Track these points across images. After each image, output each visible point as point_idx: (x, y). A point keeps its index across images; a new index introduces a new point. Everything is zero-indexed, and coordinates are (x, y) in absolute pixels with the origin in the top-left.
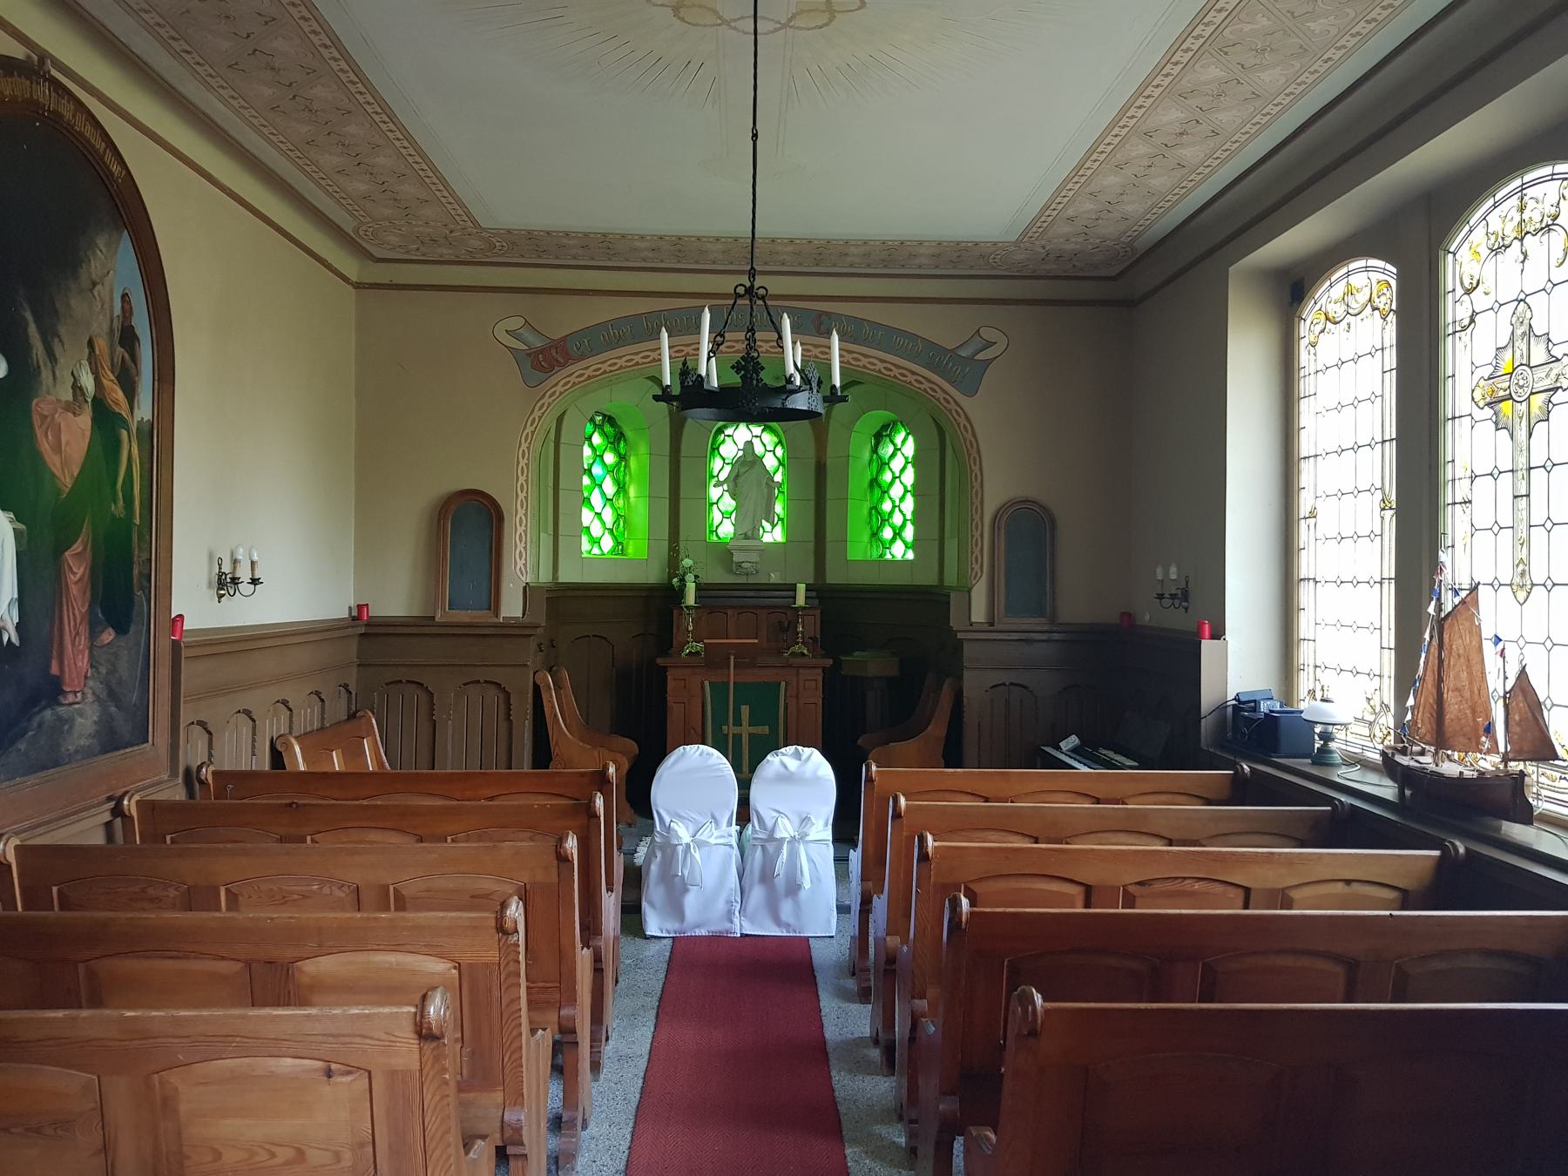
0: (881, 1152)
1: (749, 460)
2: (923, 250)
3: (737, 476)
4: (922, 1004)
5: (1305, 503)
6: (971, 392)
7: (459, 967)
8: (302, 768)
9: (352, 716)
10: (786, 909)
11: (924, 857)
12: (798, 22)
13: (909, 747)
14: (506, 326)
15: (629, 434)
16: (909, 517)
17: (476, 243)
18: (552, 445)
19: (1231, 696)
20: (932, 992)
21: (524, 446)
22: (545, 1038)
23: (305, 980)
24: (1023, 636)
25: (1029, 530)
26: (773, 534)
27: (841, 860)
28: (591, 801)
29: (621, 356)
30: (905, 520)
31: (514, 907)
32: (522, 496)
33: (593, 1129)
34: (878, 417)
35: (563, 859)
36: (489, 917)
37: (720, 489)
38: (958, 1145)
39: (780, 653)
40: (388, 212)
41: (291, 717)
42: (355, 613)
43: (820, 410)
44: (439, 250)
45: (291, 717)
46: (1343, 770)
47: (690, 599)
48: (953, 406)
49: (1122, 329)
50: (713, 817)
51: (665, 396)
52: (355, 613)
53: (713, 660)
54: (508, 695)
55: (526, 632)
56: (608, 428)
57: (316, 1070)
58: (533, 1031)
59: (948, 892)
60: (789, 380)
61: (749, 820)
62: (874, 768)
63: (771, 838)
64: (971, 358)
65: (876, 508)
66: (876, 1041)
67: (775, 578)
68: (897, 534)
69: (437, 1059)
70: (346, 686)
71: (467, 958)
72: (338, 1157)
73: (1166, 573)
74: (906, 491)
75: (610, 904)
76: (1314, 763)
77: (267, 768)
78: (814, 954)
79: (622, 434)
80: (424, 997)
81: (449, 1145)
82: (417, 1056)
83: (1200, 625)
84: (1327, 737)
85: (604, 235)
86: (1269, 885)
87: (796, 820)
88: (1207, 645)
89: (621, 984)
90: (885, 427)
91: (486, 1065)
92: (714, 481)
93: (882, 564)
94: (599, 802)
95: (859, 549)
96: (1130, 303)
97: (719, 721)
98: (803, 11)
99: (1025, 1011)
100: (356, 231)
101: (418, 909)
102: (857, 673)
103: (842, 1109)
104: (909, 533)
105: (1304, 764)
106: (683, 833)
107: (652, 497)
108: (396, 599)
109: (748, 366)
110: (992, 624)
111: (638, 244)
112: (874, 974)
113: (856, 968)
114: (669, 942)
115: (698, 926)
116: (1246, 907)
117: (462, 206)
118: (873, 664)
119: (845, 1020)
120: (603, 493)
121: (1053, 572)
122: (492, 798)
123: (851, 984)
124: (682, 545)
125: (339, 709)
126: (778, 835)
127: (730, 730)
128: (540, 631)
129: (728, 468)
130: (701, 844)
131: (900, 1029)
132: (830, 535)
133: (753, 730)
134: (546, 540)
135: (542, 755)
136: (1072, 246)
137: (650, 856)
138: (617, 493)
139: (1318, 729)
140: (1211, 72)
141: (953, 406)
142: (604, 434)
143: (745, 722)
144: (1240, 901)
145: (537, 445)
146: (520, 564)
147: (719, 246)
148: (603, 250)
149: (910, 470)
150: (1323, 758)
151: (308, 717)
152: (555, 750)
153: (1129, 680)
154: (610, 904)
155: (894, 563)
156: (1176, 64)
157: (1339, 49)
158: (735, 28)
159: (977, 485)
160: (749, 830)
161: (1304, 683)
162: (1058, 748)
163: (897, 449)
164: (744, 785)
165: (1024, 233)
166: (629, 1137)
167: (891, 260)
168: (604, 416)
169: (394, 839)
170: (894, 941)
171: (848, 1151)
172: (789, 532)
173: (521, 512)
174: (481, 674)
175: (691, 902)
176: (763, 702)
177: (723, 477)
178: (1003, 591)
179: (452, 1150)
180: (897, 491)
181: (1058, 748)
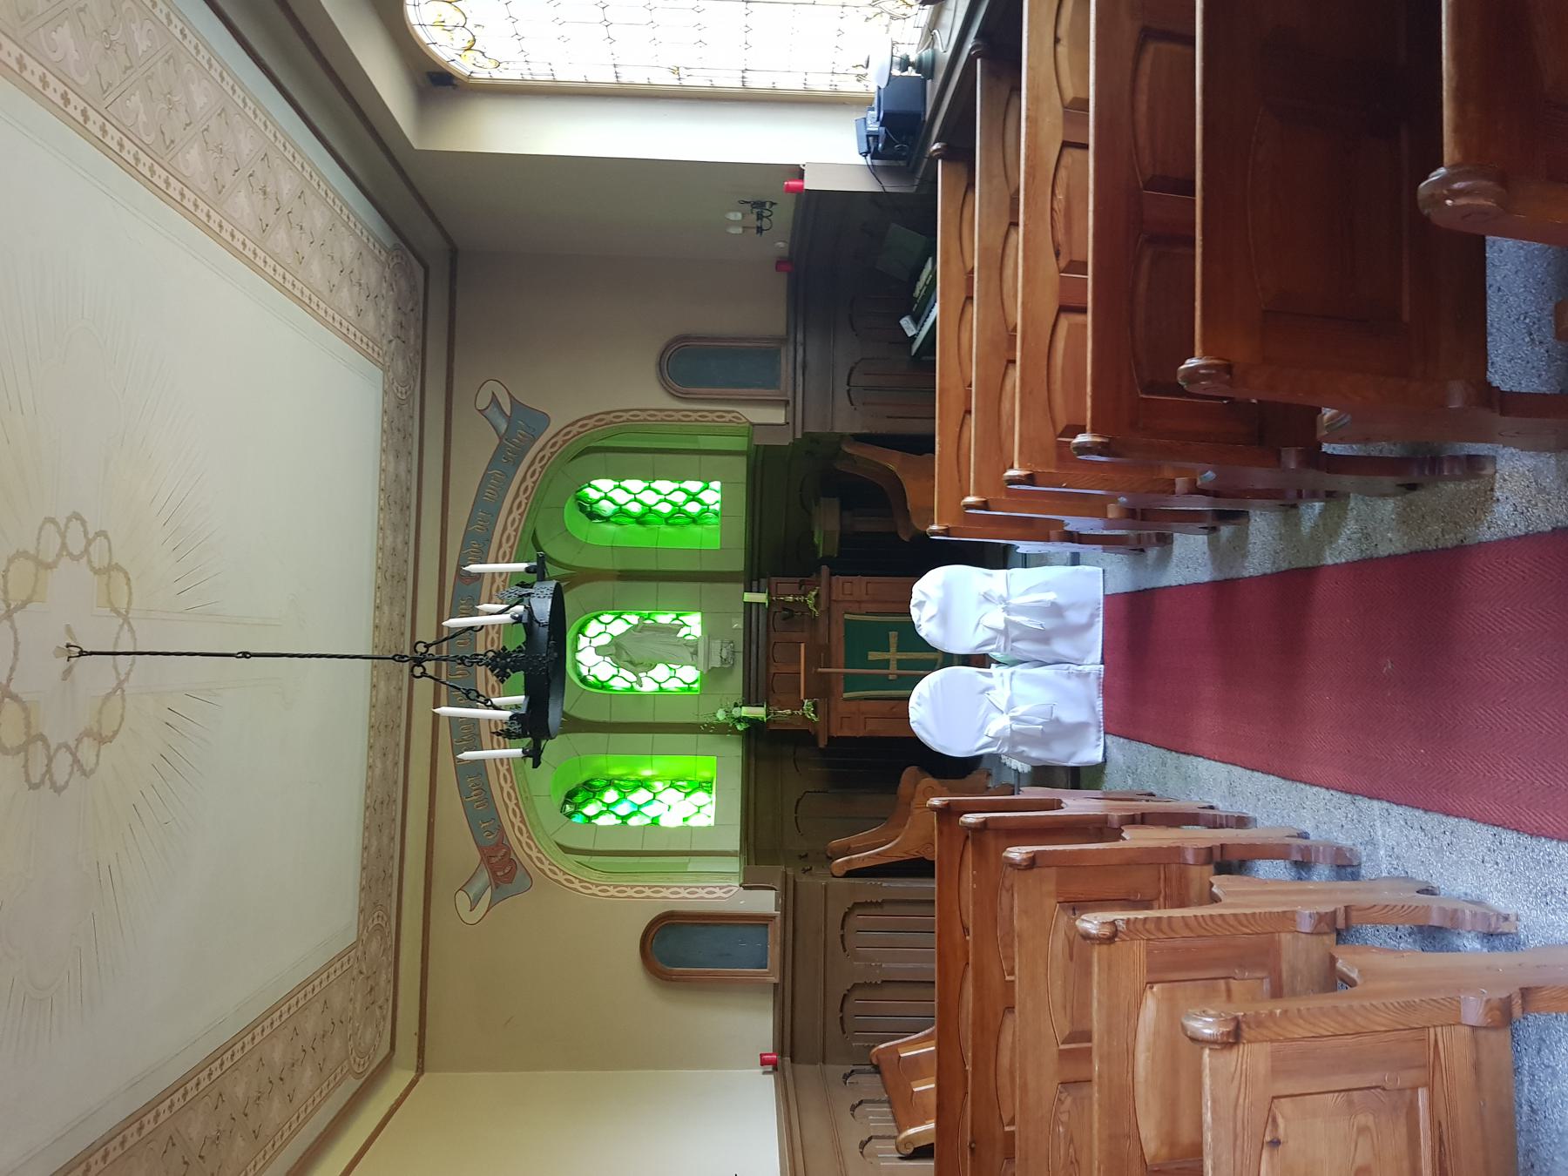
0: (1329, 529)
1: (616, 651)
2: (391, 468)
3: (631, 662)
4: (1181, 483)
5: (664, 79)
6: (546, 420)
7: (1151, 983)
8: (931, 1125)
9: (877, 1069)
10: (1076, 617)
11: (1030, 479)
12: (122, 605)
13: (912, 489)
14: (465, 911)
15: (585, 776)
16: (676, 485)
17: (374, 946)
18: (595, 859)
19: (862, 161)
20: (1167, 473)
21: (595, 890)
22: (1221, 884)
23: (1164, 1152)
24: (799, 372)
25: (690, 364)
26: (693, 625)
27: (1025, 562)
28: (969, 827)
29: (499, 789)
30: (679, 489)
31: (1088, 926)
32: (648, 892)
33: (1307, 827)
34: (572, 518)
35: (1032, 862)
36: (1097, 953)
37: (645, 680)
38: (1327, 448)
39: (814, 620)
40: (337, 1043)
41: (878, 1137)
42: (770, 1068)
43: (552, 584)
44: (382, 983)
45: (878, 1137)
46: (939, 48)
47: (759, 712)
48: (560, 439)
49: (471, 260)
50: (983, 692)
51: (535, 755)
52: (770, 1068)
53: (822, 690)
54: (856, 905)
55: (791, 886)
56: (579, 799)
57: (1271, 1157)
58: (1214, 899)
59: (1065, 455)
60: (518, 620)
61: (985, 656)
62: (935, 527)
63: (1005, 633)
64: (509, 419)
65: (666, 520)
66: (1213, 530)
67: (738, 624)
68: (694, 498)
69: (1260, 1024)
70: (846, 1077)
71: (1141, 976)
72: (1363, 1130)
73: (735, 223)
74: (649, 488)
75: (1076, 804)
76: (932, 77)
77: (932, 1163)
78: (1121, 590)
79: (585, 783)
80: (1194, 1039)
81: (1351, 1007)
82: (1256, 1046)
83: (789, 189)
84: (905, 64)
85: (367, 808)
86: (1059, 121)
87: (987, 606)
88: (810, 183)
89: (1153, 789)
90: (582, 509)
91: (1250, 953)
92: (636, 687)
93: (724, 514)
94: (971, 818)
95: (708, 537)
96: (454, 253)
97: (884, 682)
98: (109, 601)
99: (1205, 377)
100: (358, 1075)
101: (1087, 1015)
102: (838, 539)
103: (1285, 566)
104: (693, 486)
105: (932, 87)
106: (999, 724)
107: (653, 752)
108: (757, 1026)
109: (502, 664)
110: (787, 402)
111: (378, 771)
112: (1144, 530)
113: (1136, 548)
114: (1110, 739)
115: (1093, 708)
116: (1086, 147)
117: (330, 964)
118: (826, 527)
119: (1190, 560)
120: (648, 803)
121: (735, 339)
122: (966, 930)
123: (1153, 553)
124: (702, 720)
125: (869, 1084)
126: (1001, 626)
127: (893, 671)
128: (790, 872)
129: (623, 672)
130: (1011, 705)
131: (1200, 504)
132: (695, 567)
133: (893, 649)
134: (695, 864)
135: (919, 867)
136: (390, 312)
137: (1021, 757)
138: (647, 788)
139: (896, 72)
140: (193, 160)
141: (560, 439)
142: (585, 802)
143: (886, 656)
144: (1077, 153)
145: (594, 876)
146: (719, 893)
147: (382, 685)
148: (384, 811)
149: (627, 484)
150: (926, 68)
151: (877, 1119)
152: (913, 854)
153: (846, 267)
154: (1076, 804)
155: (723, 502)
156: (182, 195)
157: (170, 22)
158: (128, 674)
159: (643, 415)
160: (997, 655)
161: (849, 86)
162: (914, 338)
163: (606, 498)
164: (949, 660)
165: (375, 362)
166: (1315, 789)
167: (403, 503)
168: (566, 802)
169: (1007, 1038)
170: (1113, 511)
171: (1330, 561)
172: (691, 609)
173: (666, 893)
174: (834, 933)
175: (1069, 716)
176: (864, 638)
177: (632, 678)
178: (752, 391)
179: (1356, 1003)
180: (650, 498)
181: (914, 338)
